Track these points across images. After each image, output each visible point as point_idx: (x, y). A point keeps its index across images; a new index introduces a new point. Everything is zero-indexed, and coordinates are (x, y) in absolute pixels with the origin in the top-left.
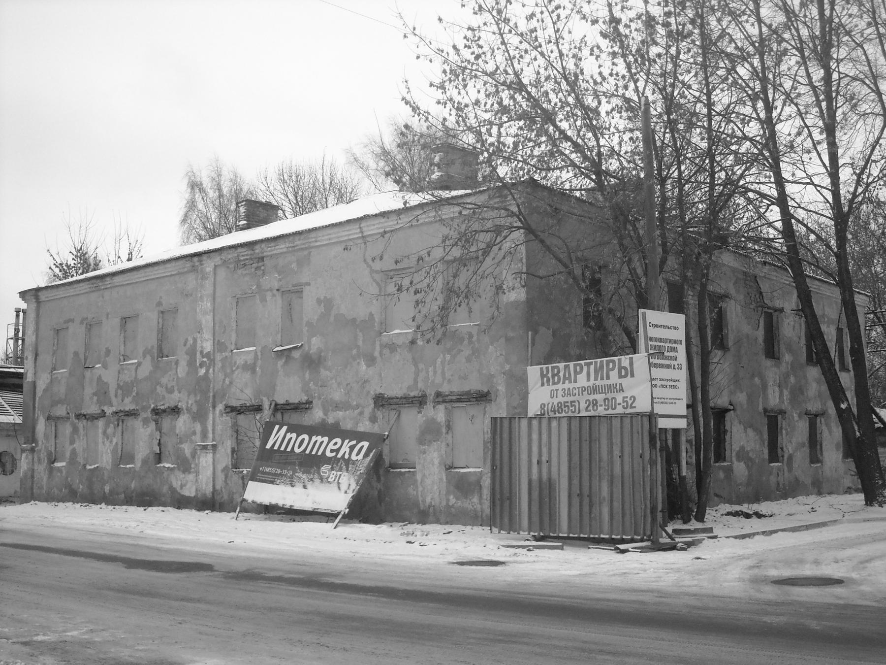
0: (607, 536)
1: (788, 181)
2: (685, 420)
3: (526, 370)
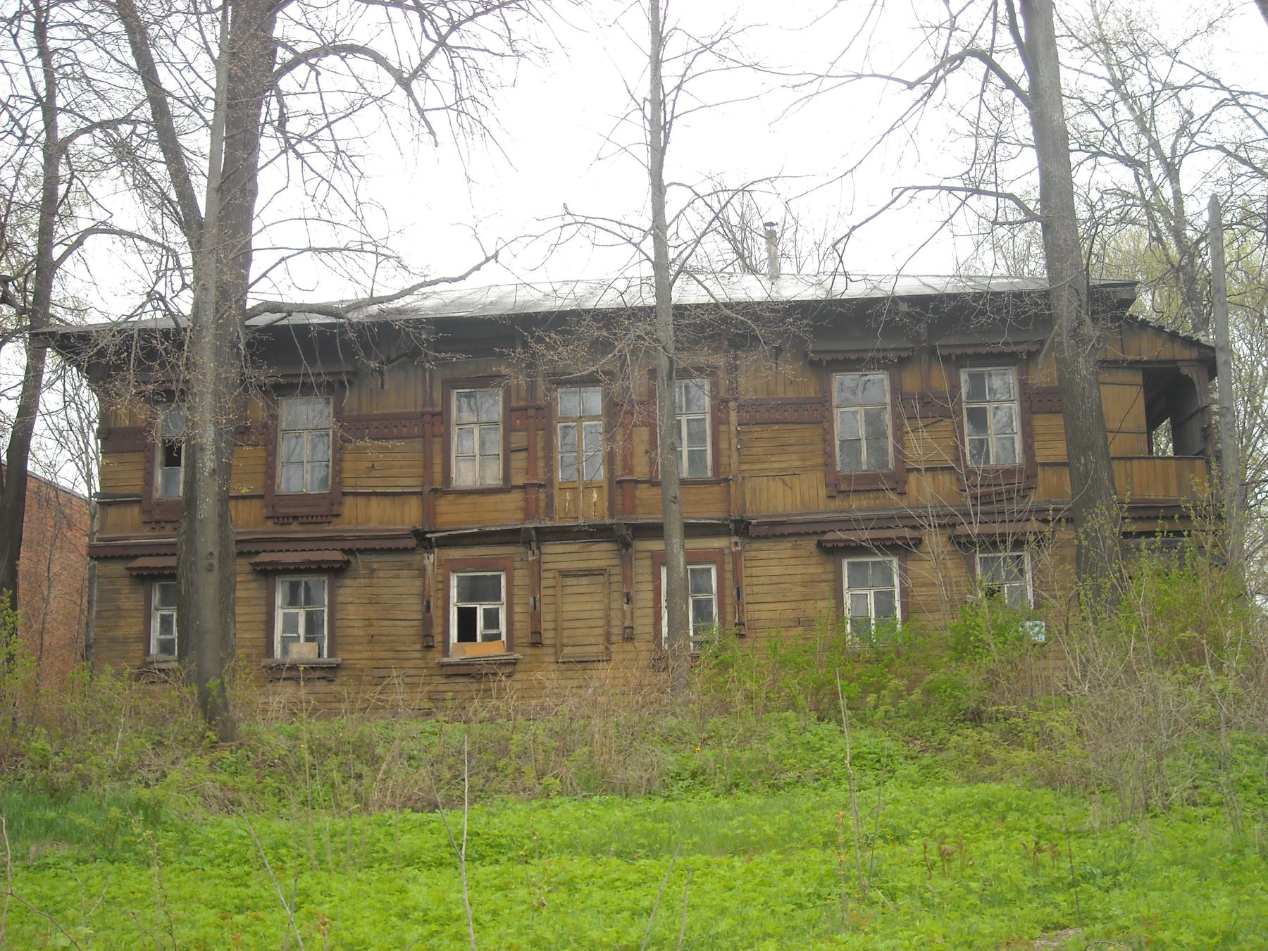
1: (1032, 146)
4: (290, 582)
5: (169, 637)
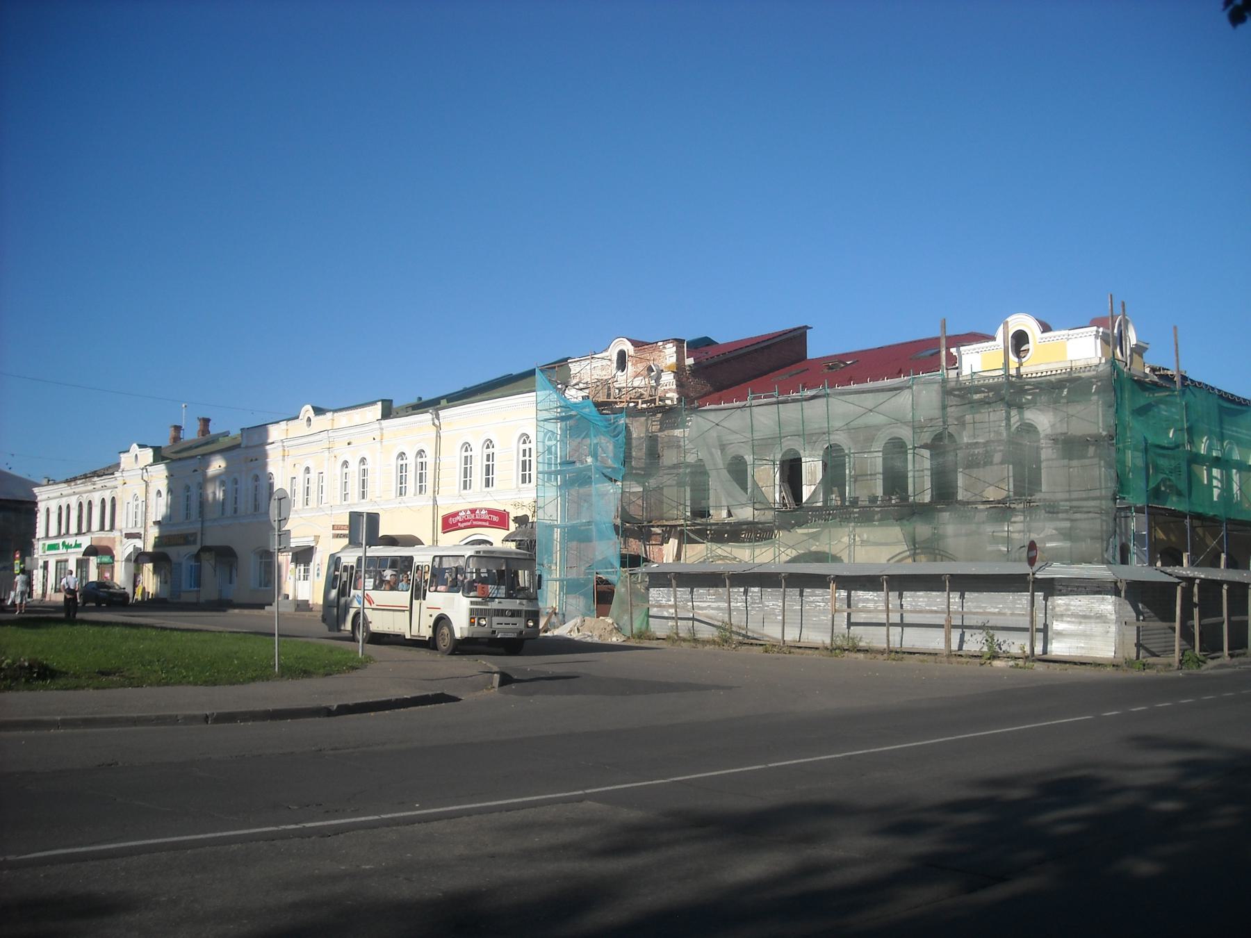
0: (688, 489)
3: (958, 591)
4: (687, 358)
5: (1207, 621)
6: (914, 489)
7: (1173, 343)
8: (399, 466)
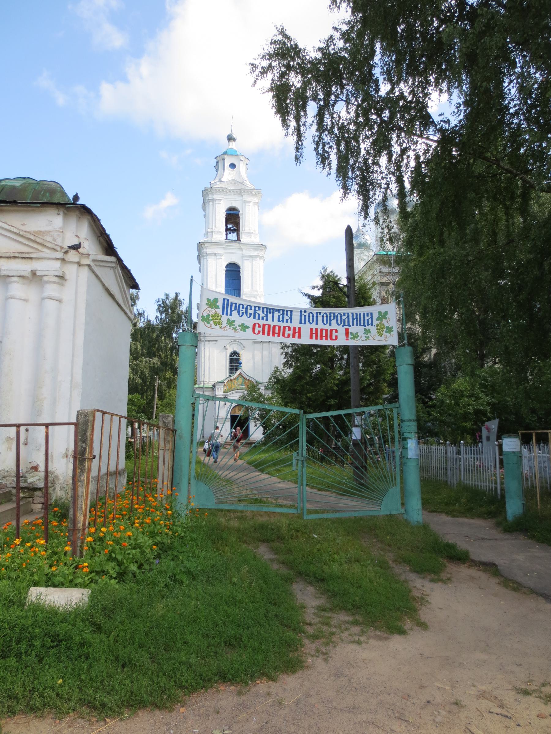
2: (73, 427)
4: (239, 295)
5: (534, 434)
6: (254, 362)
7: (104, 425)
8: (230, 304)
